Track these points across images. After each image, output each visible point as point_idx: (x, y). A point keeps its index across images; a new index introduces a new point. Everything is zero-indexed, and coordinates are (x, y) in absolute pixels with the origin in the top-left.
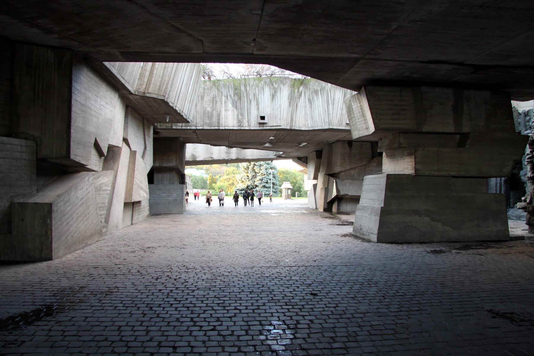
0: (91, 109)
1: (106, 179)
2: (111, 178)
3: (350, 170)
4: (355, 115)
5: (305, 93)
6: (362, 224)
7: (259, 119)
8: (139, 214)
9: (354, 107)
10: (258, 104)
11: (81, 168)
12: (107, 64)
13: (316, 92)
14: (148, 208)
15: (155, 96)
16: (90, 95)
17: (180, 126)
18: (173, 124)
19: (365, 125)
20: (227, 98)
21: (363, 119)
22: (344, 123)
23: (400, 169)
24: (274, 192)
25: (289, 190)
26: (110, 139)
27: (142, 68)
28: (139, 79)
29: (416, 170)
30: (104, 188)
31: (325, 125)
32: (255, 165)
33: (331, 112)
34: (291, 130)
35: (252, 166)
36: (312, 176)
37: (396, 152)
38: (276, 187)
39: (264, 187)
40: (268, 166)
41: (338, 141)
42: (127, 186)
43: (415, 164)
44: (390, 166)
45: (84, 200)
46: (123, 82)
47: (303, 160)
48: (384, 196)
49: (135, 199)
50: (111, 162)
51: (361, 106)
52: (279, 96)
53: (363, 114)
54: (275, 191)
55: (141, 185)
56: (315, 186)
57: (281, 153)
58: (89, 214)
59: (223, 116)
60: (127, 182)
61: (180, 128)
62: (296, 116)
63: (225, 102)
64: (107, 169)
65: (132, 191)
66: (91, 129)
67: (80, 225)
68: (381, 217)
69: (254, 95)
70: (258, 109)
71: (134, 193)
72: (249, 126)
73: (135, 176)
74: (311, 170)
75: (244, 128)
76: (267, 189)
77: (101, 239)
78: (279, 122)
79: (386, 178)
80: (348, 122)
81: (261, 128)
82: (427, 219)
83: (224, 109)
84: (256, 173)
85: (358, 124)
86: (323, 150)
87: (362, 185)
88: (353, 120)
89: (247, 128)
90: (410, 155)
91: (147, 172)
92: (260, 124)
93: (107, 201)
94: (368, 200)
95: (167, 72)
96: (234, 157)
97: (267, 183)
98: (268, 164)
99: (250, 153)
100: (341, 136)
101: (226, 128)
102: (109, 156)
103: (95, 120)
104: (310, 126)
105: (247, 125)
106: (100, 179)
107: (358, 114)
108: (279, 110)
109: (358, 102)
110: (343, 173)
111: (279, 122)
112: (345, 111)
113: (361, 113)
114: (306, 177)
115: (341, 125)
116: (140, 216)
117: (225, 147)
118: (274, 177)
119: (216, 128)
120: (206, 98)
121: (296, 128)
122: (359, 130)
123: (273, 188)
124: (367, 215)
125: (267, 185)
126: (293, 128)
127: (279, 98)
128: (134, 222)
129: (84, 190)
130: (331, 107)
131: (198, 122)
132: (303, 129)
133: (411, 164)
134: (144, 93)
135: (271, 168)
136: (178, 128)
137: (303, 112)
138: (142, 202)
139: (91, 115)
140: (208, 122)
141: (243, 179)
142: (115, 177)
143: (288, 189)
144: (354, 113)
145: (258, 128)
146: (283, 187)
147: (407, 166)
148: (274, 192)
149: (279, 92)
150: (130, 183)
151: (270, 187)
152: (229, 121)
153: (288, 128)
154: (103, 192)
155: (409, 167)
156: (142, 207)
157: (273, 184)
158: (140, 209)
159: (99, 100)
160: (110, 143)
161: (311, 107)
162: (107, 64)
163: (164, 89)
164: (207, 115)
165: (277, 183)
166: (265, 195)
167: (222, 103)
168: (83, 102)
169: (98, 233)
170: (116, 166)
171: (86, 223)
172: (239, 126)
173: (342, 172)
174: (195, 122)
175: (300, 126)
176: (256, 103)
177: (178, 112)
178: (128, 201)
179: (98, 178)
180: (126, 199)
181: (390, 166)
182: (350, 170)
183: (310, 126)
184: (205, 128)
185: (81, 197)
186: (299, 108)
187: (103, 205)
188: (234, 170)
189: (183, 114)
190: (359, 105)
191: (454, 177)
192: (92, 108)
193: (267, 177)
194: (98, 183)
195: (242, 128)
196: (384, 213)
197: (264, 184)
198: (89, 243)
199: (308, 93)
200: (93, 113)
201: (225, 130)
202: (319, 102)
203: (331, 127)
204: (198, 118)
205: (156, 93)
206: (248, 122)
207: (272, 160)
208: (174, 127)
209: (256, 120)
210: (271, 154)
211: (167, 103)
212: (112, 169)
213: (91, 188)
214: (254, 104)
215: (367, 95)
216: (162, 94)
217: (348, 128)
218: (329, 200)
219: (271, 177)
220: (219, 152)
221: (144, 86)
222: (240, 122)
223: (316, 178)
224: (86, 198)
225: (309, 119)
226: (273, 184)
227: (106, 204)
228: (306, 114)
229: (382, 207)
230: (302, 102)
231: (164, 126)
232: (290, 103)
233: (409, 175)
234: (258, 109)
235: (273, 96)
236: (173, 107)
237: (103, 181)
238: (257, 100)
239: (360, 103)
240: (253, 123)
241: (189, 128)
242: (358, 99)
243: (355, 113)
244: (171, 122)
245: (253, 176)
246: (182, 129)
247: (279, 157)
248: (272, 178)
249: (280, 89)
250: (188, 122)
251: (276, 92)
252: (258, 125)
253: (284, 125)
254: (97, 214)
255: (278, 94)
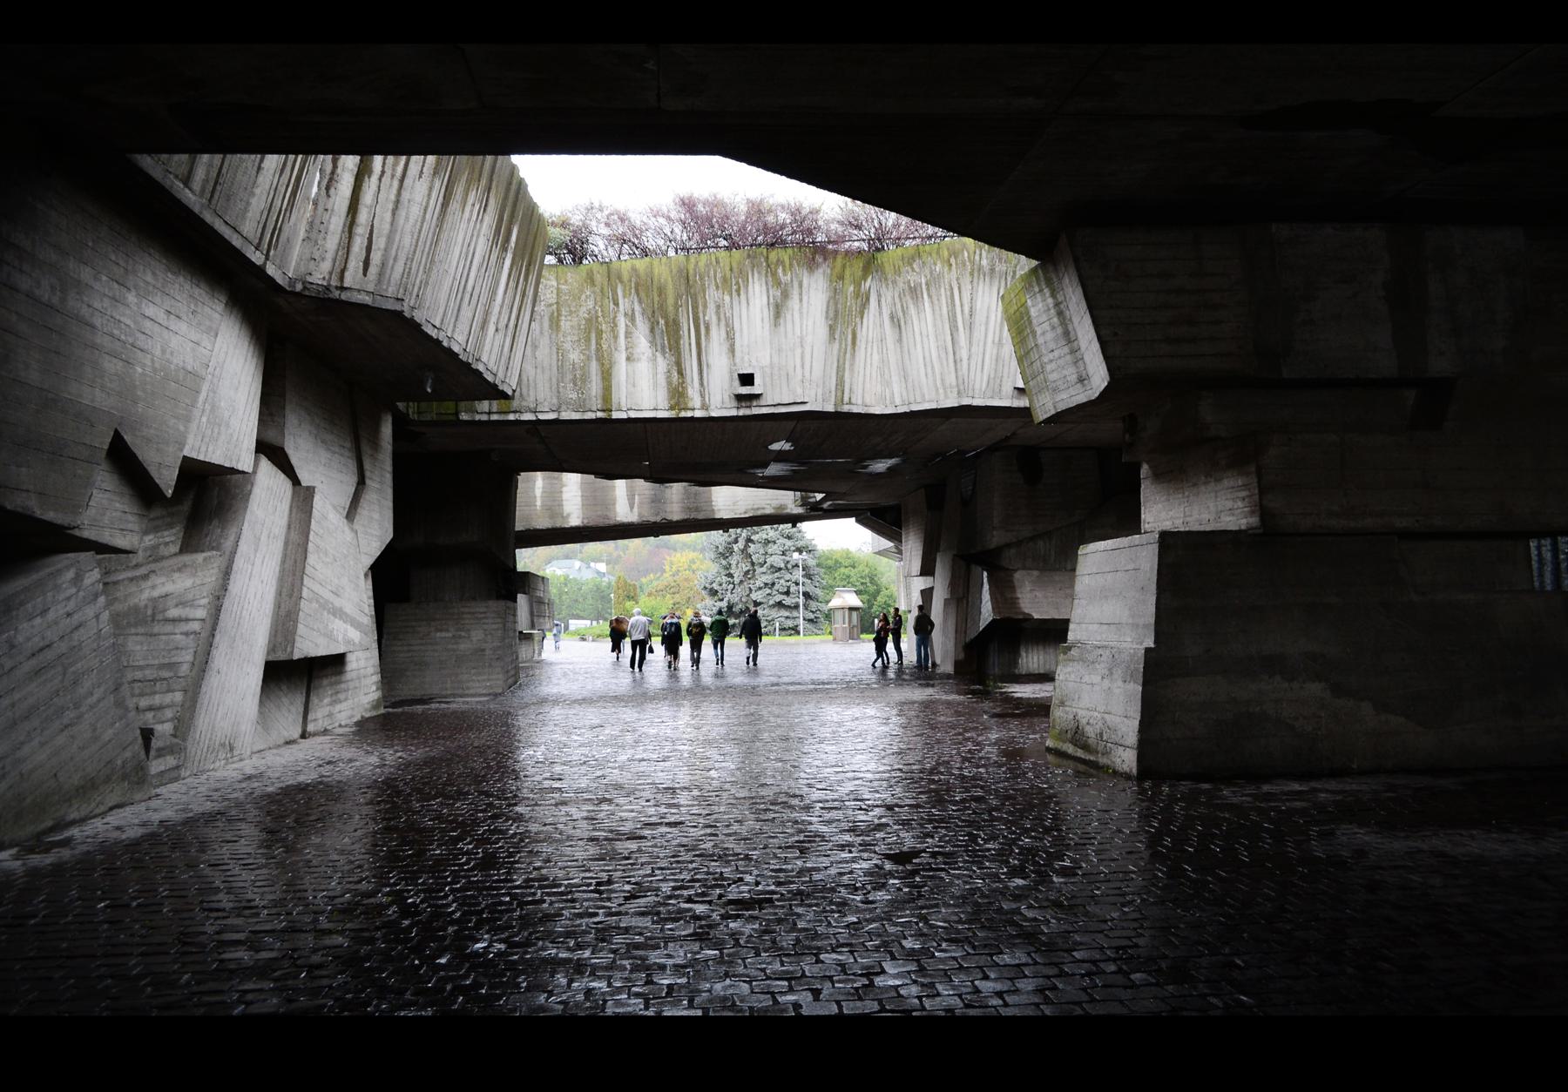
0: (93, 327)
1: (180, 583)
2: (210, 576)
3: (1032, 539)
4: (1040, 340)
5: (879, 296)
6: (1081, 713)
7: (737, 382)
8: (334, 703)
9: (1033, 312)
10: (730, 337)
11: (63, 541)
12: (147, 162)
13: (914, 291)
14: (377, 678)
15: (367, 300)
16: (86, 274)
17: (485, 410)
18: (462, 405)
19: (1077, 372)
20: (633, 320)
21: (1066, 349)
22: (1008, 388)
23: (1206, 516)
24: (810, 621)
25: (855, 614)
26: (190, 440)
27: (315, 204)
28: (307, 239)
29: (1264, 512)
30: (173, 613)
31: (946, 397)
32: (749, 540)
33: (964, 354)
34: (837, 415)
35: (741, 544)
36: (916, 566)
37: (1184, 465)
38: (813, 605)
39: (780, 605)
40: (789, 543)
41: (993, 449)
42: (278, 606)
43: (1261, 493)
44: (1161, 512)
45: (49, 655)
46: (236, 242)
47: (885, 520)
48: (1153, 609)
49: (310, 644)
50: (215, 522)
51: (1057, 305)
52: (796, 307)
53: (1066, 333)
54: (812, 616)
55: (337, 602)
56: (927, 594)
57: (819, 496)
58: (77, 706)
59: (623, 378)
60: (279, 593)
61: (485, 418)
62: (852, 370)
63: (628, 334)
64: (197, 549)
65: (296, 622)
66: (96, 397)
67: (26, 749)
68: (1144, 685)
69: (718, 307)
70: (732, 350)
71: (301, 629)
72: (705, 407)
73: (308, 570)
74: (913, 548)
75: (689, 414)
76: (787, 614)
77: (138, 797)
78: (799, 391)
79: (1156, 547)
80: (1021, 385)
81: (742, 412)
82: (1315, 688)
83: (624, 356)
84: (753, 564)
85: (1049, 368)
86: (953, 485)
87: (1072, 586)
88: (1034, 356)
89: (698, 414)
90: (1237, 463)
91: (369, 561)
92: (740, 398)
93: (189, 658)
94: (1096, 627)
95: (407, 218)
96: (676, 514)
97: (787, 593)
98: (789, 538)
99: (728, 499)
100: (1003, 429)
101: (633, 415)
102: (201, 501)
103: (111, 366)
104: (898, 402)
105: (697, 402)
106: (154, 580)
107: (1050, 336)
108: (798, 351)
109: (1047, 291)
110: (1013, 551)
111: (799, 391)
112: (1008, 348)
113: (1059, 330)
114: (896, 572)
115: (999, 394)
116: (338, 707)
117: (641, 481)
118: (808, 576)
119: (600, 415)
120: (565, 324)
121: (855, 410)
122: (1055, 390)
123: (806, 607)
124: (1096, 679)
125: (788, 601)
126: (846, 408)
127: (797, 315)
128: (311, 728)
129: (51, 615)
130: (958, 329)
131: (541, 397)
132: (877, 410)
133: (1244, 494)
134: (327, 288)
135: (800, 550)
136: (477, 417)
137: (876, 357)
138: (350, 658)
139: (94, 347)
140: (574, 396)
141: (715, 586)
142: (227, 573)
143: (851, 609)
144: (1034, 333)
145: (734, 413)
146: (835, 602)
147: (1229, 504)
148: (810, 621)
149: (795, 296)
150: (291, 596)
151: (796, 607)
152: (641, 391)
153: (830, 408)
154: (168, 628)
155: (1240, 504)
156: (348, 676)
157: (807, 595)
158: (340, 682)
159: (131, 298)
160: (186, 452)
161: (900, 340)
162: (147, 162)
163: (397, 274)
164: (569, 377)
165: (819, 592)
166: (783, 629)
167: (616, 338)
168: (44, 293)
169: (125, 777)
170: (232, 538)
171: (61, 740)
172: (672, 408)
173: (1008, 546)
174: (532, 398)
175: (868, 401)
176: (723, 335)
177: (463, 357)
178: (281, 656)
179: (145, 577)
180: (272, 648)
181: (1161, 512)
182: (1032, 539)
183: (898, 402)
184: (565, 416)
185: (37, 642)
186: (861, 344)
187: (166, 674)
188: (693, 561)
189: (481, 368)
190: (1050, 301)
191: (1405, 535)
192: (97, 321)
193: (788, 576)
194: (145, 595)
195: (683, 414)
196: (1158, 671)
197: (778, 598)
198: (74, 815)
199: (888, 295)
200: (100, 339)
201: (629, 420)
202: (926, 322)
203: (966, 402)
204: (540, 385)
205: (371, 288)
206: (702, 396)
207: (794, 520)
208: (464, 417)
209: (726, 386)
210: (787, 500)
211: (414, 326)
212: (217, 548)
213: (90, 612)
214: (717, 336)
215: (1076, 261)
216: (391, 291)
217: (1022, 403)
218: (972, 635)
219: (798, 575)
220: (626, 498)
221: (326, 266)
222: (677, 394)
223: (927, 570)
224: (63, 647)
225: (895, 378)
226: (807, 595)
227: (185, 669)
228: (884, 361)
229: (1148, 650)
230: (873, 324)
231: (433, 411)
232: (832, 329)
233: (1239, 532)
234: (732, 350)
235: (778, 311)
236: (438, 342)
237: (169, 588)
238: (727, 325)
239: (1053, 295)
240: (719, 398)
241: (511, 417)
242: (1049, 283)
243: (1039, 331)
244: (438, 396)
245: (747, 573)
246: (489, 422)
247: (816, 512)
248: (801, 580)
249: (801, 286)
250: (503, 396)
251: (786, 295)
252: (734, 404)
253: (818, 400)
254: (120, 704)
255: (794, 303)
